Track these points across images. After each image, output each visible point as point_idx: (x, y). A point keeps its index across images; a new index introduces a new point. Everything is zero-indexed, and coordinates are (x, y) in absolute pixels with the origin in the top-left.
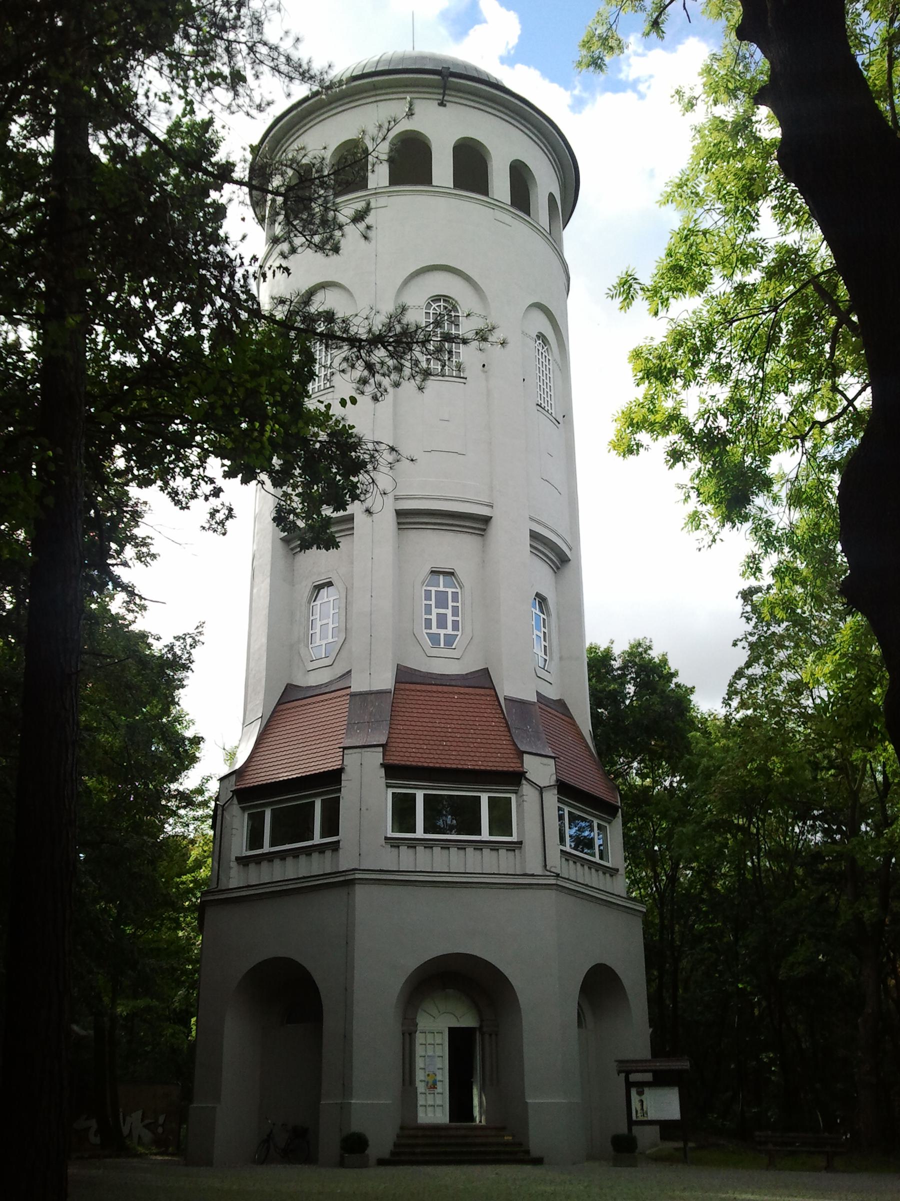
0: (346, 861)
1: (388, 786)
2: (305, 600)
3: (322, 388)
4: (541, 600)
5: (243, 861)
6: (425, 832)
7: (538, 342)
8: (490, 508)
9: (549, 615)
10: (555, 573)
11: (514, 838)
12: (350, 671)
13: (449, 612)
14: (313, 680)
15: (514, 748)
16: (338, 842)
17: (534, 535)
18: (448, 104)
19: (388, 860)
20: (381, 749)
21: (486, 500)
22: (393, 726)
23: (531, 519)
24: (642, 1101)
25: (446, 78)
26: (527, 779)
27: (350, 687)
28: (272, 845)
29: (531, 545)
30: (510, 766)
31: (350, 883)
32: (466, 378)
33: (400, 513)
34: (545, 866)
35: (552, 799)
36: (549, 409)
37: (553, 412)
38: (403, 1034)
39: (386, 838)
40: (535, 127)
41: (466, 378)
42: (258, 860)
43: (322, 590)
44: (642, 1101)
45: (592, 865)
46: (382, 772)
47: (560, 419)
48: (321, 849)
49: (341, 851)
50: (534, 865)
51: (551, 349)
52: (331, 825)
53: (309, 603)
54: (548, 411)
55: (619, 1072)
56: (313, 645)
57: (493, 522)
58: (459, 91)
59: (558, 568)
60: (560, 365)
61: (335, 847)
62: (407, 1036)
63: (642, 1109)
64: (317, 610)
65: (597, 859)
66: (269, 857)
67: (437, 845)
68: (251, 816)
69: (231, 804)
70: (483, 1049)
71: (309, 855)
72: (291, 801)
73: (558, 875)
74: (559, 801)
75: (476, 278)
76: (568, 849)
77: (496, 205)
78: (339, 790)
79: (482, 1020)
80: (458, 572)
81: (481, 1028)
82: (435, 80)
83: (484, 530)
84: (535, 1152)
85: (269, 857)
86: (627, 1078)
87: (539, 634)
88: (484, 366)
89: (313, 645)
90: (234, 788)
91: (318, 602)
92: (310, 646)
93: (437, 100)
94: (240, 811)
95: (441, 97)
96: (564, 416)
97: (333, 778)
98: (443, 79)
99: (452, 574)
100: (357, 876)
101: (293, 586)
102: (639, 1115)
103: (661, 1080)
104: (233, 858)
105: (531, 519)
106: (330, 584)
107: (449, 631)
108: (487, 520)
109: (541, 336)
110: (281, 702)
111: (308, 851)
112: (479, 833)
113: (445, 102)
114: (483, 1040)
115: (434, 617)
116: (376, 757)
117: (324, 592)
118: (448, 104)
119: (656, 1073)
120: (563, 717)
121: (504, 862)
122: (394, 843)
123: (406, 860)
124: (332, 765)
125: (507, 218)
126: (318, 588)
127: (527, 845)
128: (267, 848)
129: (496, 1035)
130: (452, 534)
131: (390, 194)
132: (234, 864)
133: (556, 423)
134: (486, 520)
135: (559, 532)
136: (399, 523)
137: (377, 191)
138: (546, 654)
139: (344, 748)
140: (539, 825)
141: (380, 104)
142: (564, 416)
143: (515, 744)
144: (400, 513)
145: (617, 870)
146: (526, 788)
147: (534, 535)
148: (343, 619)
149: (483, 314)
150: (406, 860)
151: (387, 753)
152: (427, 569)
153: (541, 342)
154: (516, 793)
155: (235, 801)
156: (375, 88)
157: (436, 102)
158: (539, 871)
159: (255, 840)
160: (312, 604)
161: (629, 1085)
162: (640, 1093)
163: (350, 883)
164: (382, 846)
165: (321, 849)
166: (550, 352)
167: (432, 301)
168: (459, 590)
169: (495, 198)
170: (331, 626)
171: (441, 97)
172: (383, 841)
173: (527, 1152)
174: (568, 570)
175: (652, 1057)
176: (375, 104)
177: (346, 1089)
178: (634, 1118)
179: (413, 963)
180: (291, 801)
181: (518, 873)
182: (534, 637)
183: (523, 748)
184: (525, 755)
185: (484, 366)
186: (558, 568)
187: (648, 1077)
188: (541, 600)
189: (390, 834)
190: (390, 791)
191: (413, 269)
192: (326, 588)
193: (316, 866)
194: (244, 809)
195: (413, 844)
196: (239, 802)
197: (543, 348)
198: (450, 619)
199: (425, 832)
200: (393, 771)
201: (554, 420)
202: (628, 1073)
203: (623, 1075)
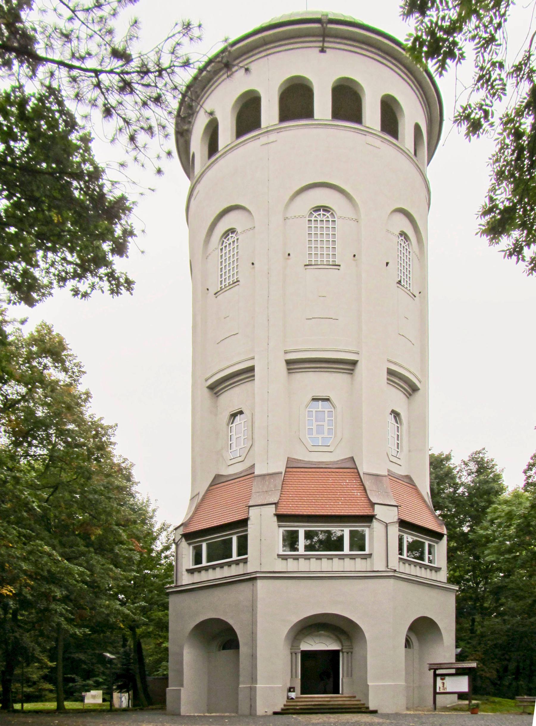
0: (251, 567)
1: (280, 526)
2: (225, 425)
3: (231, 283)
4: (396, 415)
5: (191, 571)
6: (305, 551)
7: (401, 238)
8: (357, 355)
9: (401, 424)
10: (408, 398)
11: (367, 552)
12: (254, 464)
13: (326, 424)
14: (231, 471)
15: (368, 501)
16: (247, 558)
17: (390, 372)
18: (327, 50)
19: (280, 566)
20: (274, 506)
21: (355, 349)
22: (283, 493)
23: (389, 361)
24: (443, 683)
25: (325, 25)
26: (376, 519)
27: (254, 473)
28: (209, 561)
29: (388, 379)
30: (366, 512)
31: (255, 579)
32: (339, 266)
33: (289, 362)
34: (387, 566)
35: (394, 531)
36: (408, 287)
37: (411, 289)
38: (291, 654)
39: (279, 556)
40: (423, 91)
41: (339, 266)
42: (199, 570)
43: (237, 417)
44: (443, 683)
45: (426, 567)
46: (275, 519)
47: (417, 294)
48: (237, 563)
49: (248, 563)
50: (378, 564)
51: (412, 244)
52: (243, 549)
53: (228, 425)
54: (403, 286)
55: (430, 669)
56: (231, 451)
57: (359, 364)
58: (336, 37)
59: (410, 395)
60: (418, 256)
61: (245, 561)
62: (294, 654)
63: (443, 686)
64: (234, 429)
65: (426, 562)
66: (206, 569)
67: (313, 558)
68: (195, 548)
69: (181, 542)
70: (343, 659)
71: (230, 566)
72: (218, 538)
73: (395, 571)
74: (400, 530)
75: (343, 186)
76: (405, 557)
77: (368, 132)
78: (247, 530)
79: (342, 646)
80: (332, 398)
81: (342, 649)
82: (316, 28)
83: (353, 370)
84: (372, 708)
85: (206, 569)
86: (435, 672)
87: (393, 435)
88: (354, 256)
89: (231, 451)
90: (182, 533)
91: (234, 425)
92: (230, 451)
93: (319, 47)
94: (187, 546)
95: (321, 44)
96: (420, 293)
97: (244, 523)
98: (322, 25)
99: (328, 400)
100: (258, 575)
101: (216, 415)
102: (441, 689)
103: (460, 672)
104: (184, 570)
105: (389, 361)
106: (241, 413)
107: (326, 435)
108: (354, 363)
109: (403, 234)
110: (213, 484)
111: (229, 564)
112: (342, 550)
113: (325, 49)
114: (343, 655)
115: (314, 428)
116: (272, 510)
117: (238, 418)
118: (327, 50)
119: (457, 669)
120: (409, 485)
121: (360, 565)
122: (284, 558)
123: (291, 566)
124: (243, 517)
125: (377, 142)
126: (234, 416)
127: (375, 556)
128: (204, 563)
129: (352, 653)
130: (327, 374)
131: (278, 130)
132: (185, 573)
133: (413, 297)
134: (354, 363)
135: (412, 370)
136: (288, 369)
137: (269, 129)
138: (398, 448)
139: (250, 507)
140: (385, 544)
141: (270, 57)
142: (420, 293)
143: (369, 500)
144: (289, 362)
145: (440, 569)
146: (375, 523)
147: (390, 372)
148: (250, 432)
149: (354, 217)
150: (291, 566)
151: (278, 508)
152: (310, 398)
153: (403, 238)
154: (369, 527)
155: (183, 540)
156: (265, 43)
157: (318, 50)
158: (383, 568)
159: (198, 559)
160: (230, 426)
161: (435, 675)
162: (442, 679)
163: (255, 579)
164: (275, 559)
165: (237, 563)
166: (410, 247)
167: (314, 211)
168: (333, 410)
169: (367, 126)
170: (243, 438)
171: (321, 44)
172: (276, 557)
173: (368, 708)
174: (418, 396)
175: (456, 661)
176: (266, 58)
177: (254, 679)
178: (438, 691)
179: (295, 619)
180: (218, 538)
181: (368, 570)
182: (389, 437)
183: (374, 500)
184: (376, 506)
185: (354, 256)
186: (410, 395)
187: (453, 671)
188: (396, 415)
189: (281, 553)
190: (281, 530)
191: (298, 188)
192: (239, 415)
193: (234, 571)
194: (189, 544)
195: (296, 558)
196: (186, 540)
197: (405, 243)
198: (326, 428)
199: (305, 551)
200: (281, 518)
201: (411, 294)
202: (435, 670)
203: (432, 671)
